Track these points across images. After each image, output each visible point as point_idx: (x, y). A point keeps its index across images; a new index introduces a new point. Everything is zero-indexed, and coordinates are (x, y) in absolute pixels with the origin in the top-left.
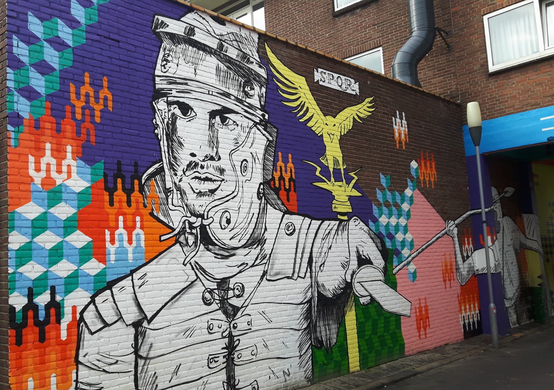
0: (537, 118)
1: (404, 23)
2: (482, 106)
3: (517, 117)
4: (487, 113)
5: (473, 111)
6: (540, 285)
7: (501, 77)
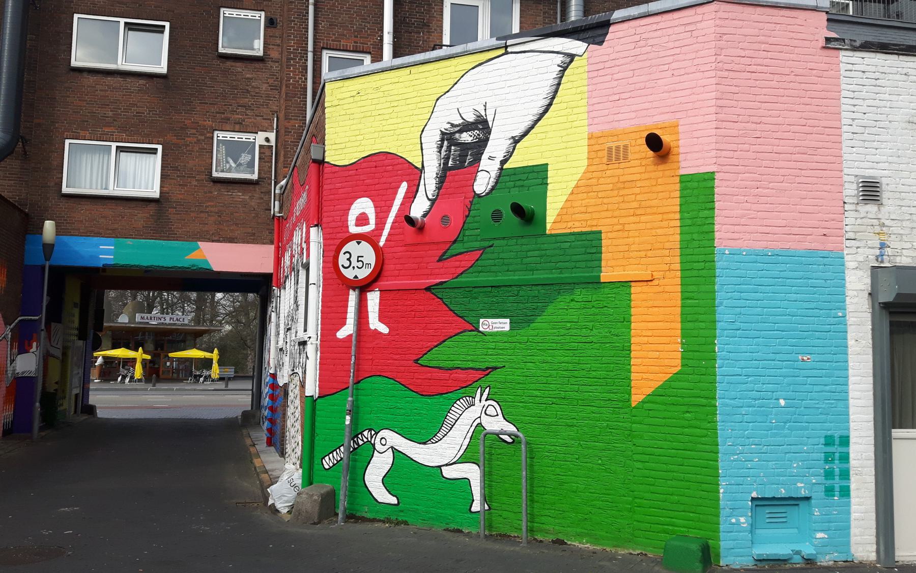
0: (97, 245)
1: (791, 467)
2: (57, 226)
3: (81, 240)
4: (59, 231)
5: (49, 226)
6: (56, 390)
7: (73, 200)
